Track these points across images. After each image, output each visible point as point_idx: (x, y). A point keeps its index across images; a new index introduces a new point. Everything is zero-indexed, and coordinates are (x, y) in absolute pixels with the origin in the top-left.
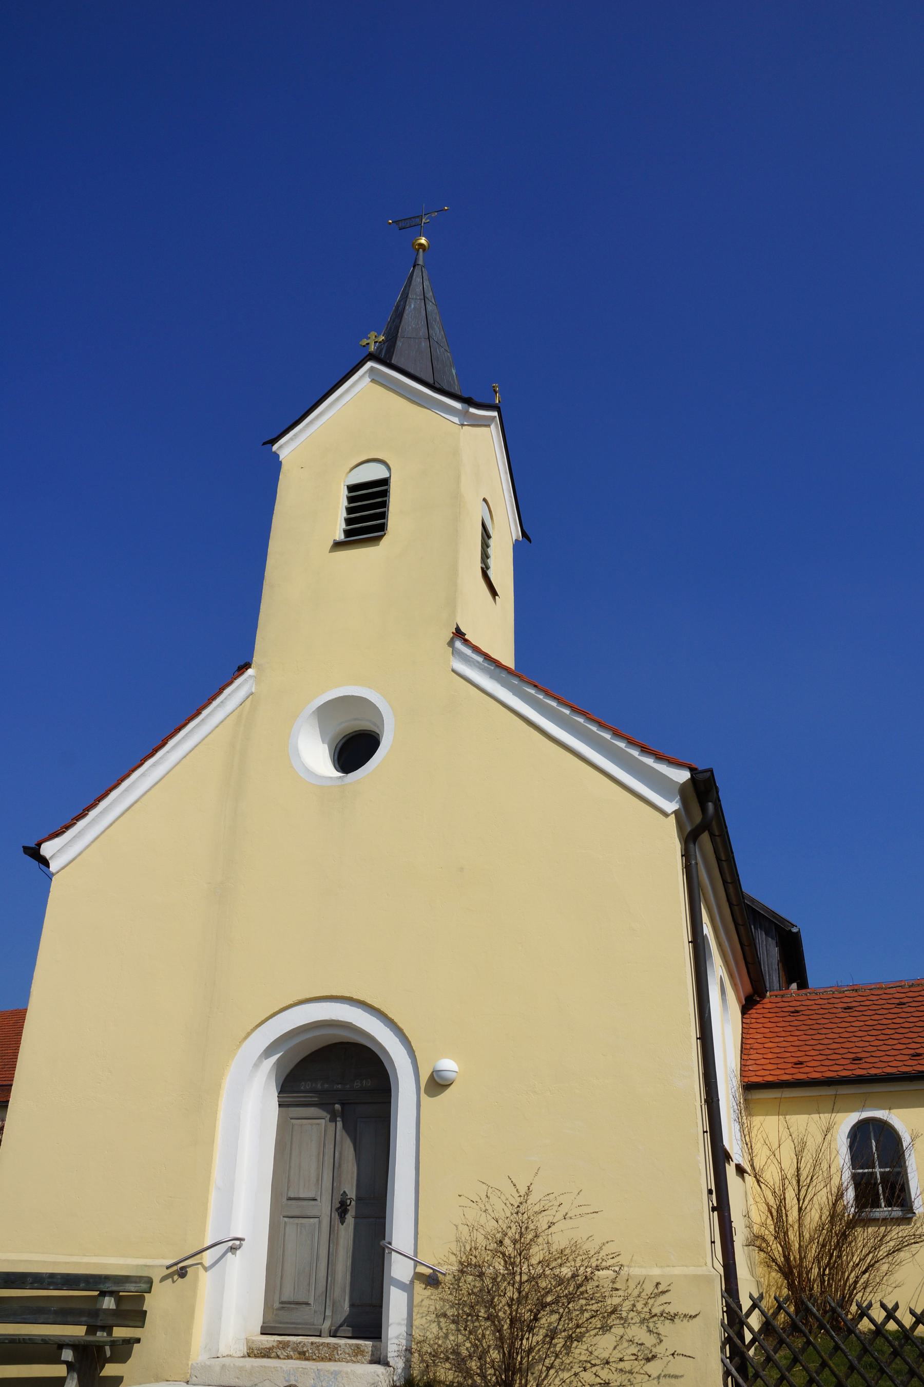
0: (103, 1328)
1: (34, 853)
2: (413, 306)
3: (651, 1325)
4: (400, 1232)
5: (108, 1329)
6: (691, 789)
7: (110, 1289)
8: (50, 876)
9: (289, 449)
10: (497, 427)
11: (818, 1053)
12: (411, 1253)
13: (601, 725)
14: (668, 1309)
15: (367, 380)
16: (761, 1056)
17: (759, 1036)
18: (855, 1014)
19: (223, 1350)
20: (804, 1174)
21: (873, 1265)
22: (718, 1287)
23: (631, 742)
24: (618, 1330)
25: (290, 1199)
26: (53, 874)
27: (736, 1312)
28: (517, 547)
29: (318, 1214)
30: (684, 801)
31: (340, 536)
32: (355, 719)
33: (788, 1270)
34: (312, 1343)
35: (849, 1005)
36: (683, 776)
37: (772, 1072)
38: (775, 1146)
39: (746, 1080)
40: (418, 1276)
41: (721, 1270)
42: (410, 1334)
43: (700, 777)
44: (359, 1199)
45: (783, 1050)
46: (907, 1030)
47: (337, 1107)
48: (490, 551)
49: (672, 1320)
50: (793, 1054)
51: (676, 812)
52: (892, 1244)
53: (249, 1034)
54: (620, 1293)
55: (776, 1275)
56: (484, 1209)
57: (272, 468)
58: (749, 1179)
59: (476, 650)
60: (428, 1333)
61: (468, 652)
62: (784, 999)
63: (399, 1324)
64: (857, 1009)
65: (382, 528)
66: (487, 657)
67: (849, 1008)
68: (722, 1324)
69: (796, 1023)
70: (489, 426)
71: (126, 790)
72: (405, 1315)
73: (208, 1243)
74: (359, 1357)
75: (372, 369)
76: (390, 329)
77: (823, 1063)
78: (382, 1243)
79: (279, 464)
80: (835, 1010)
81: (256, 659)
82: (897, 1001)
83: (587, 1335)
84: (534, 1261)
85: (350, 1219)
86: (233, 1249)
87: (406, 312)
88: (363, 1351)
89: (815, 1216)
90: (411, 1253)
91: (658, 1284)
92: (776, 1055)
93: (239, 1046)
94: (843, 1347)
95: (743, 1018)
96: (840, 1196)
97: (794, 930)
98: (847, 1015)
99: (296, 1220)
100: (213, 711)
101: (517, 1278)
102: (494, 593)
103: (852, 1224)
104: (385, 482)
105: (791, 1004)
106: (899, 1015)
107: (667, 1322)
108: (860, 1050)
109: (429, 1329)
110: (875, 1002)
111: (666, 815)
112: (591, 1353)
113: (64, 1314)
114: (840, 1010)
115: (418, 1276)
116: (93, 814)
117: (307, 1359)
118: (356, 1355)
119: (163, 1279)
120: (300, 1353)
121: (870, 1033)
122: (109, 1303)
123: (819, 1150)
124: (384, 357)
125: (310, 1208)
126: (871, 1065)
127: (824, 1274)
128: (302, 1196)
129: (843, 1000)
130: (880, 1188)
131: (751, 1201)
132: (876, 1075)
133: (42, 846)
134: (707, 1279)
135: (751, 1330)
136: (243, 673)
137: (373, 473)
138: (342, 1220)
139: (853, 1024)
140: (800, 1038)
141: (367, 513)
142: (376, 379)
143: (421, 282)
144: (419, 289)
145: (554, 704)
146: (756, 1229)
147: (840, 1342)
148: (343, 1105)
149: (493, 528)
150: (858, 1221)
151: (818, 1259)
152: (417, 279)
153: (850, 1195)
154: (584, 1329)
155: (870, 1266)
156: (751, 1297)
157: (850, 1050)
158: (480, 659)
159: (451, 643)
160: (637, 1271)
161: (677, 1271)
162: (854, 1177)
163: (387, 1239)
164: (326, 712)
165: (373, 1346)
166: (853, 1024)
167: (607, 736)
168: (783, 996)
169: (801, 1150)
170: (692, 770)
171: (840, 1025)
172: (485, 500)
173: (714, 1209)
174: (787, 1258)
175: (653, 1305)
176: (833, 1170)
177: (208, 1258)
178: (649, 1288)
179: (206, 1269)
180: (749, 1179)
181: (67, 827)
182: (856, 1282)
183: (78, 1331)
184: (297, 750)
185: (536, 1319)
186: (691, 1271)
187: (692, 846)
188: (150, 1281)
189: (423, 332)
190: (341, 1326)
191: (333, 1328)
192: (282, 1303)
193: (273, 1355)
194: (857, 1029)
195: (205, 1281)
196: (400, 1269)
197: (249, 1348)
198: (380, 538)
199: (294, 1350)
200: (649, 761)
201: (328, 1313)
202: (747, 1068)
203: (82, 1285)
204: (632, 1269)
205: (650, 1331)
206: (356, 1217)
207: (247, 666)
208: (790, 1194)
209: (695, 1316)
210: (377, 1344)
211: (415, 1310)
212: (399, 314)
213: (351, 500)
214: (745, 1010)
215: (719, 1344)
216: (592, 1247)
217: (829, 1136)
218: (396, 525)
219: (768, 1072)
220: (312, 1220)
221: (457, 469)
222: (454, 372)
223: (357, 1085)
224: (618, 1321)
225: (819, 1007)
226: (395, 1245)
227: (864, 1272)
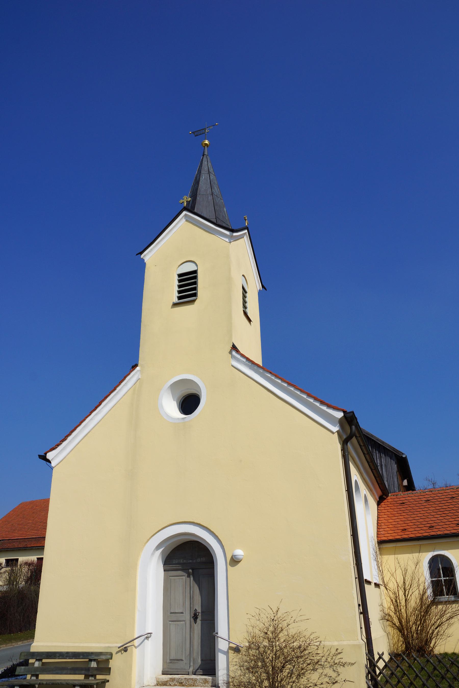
0: (92, 676)
1: (44, 458)
2: (204, 177)
3: (335, 668)
4: (222, 629)
5: (94, 676)
6: (344, 420)
7: (94, 658)
8: (52, 468)
9: (149, 256)
10: (247, 237)
11: (413, 524)
12: (227, 638)
13: (302, 391)
14: (342, 660)
15: (184, 220)
16: (387, 526)
17: (386, 516)
18: (431, 503)
19: (146, 683)
20: (407, 584)
21: (440, 625)
22: (364, 650)
23: (316, 399)
24: (320, 671)
25: (171, 613)
26: (53, 468)
27: (372, 661)
28: (260, 293)
29: (185, 620)
30: (342, 426)
31: (176, 300)
32: (188, 389)
33: (402, 629)
34: (185, 679)
35: (428, 499)
36: (340, 415)
37: (392, 535)
38: (394, 571)
39: (380, 539)
40: (230, 648)
41: (365, 640)
42: (228, 675)
43: (348, 415)
44: (202, 612)
45: (397, 523)
46: (455, 511)
47: (190, 571)
48: (247, 299)
49: (343, 666)
50: (401, 525)
51: (338, 432)
52: (448, 615)
53: (148, 540)
54: (319, 655)
55: (396, 631)
56: (258, 619)
57: (141, 266)
58: (382, 588)
59: (243, 356)
60: (236, 674)
61: (238, 356)
62: (397, 497)
63: (223, 669)
64: (432, 501)
65: (195, 295)
66: (248, 359)
67: (428, 501)
68: (366, 666)
69: (403, 509)
70: (243, 237)
71: (84, 427)
72: (226, 666)
73: (136, 637)
74: (206, 684)
75: (186, 215)
76: (193, 190)
77: (415, 529)
78: (214, 633)
79: (144, 264)
80: (421, 502)
81: (140, 362)
82: (450, 496)
83: (307, 673)
84: (282, 640)
85: (199, 621)
86: (147, 638)
87: (201, 181)
88: (208, 682)
89: (414, 601)
90: (227, 638)
91: (337, 649)
92: (393, 526)
93: (144, 546)
94: (420, 675)
95: (378, 507)
96: (424, 593)
97: (404, 456)
98: (427, 504)
99: (175, 623)
100: (122, 388)
101: (275, 648)
102: (250, 320)
103: (429, 607)
104: (195, 272)
105: (401, 499)
106: (452, 504)
107: (341, 667)
108: (433, 522)
109: (236, 672)
110: (440, 497)
111: (333, 433)
112: (308, 681)
113: (74, 670)
114: (424, 502)
115: (230, 648)
116: (69, 438)
117: (183, 686)
118: (205, 683)
119: (117, 653)
120: (180, 683)
121: (437, 513)
122: (94, 665)
123: (413, 573)
124: (191, 208)
125: (181, 617)
126: (438, 530)
127: (418, 630)
128: (177, 611)
129: (425, 496)
130: (444, 587)
131: (383, 597)
132: (440, 535)
133: (47, 454)
134: (359, 646)
135: (379, 668)
136: (135, 369)
137: (189, 268)
138: (195, 622)
139: (430, 509)
140: (405, 517)
141: (188, 287)
142: (188, 220)
143: (207, 164)
144: (206, 168)
145: (279, 381)
146: (386, 611)
147: (418, 673)
148: (193, 569)
149: (248, 288)
150: (434, 603)
151: (415, 623)
152: (205, 163)
153: (429, 592)
154: (305, 670)
155: (439, 626)
156: (378, 654)
157: (428, 522)
158: (244, 360)
159: (230, 352)
160: (327, 643)
161: (345, 643)
162: (432, 582)
163: (216, 631)
164: (175, 386)
165: (212, 679)
166: (430, 509)
167: (305, 396)
168: (397, 495)
169: (408, 571)
170: (344, 412)
171: (424, 510)
172: (243, 275)
173: (361, 613)
174: (400, 622)
175: (335, 659)
176: (420, 582)
177: (136, 643)
178: (333, 651)
179: (136, 647)
180: (382, 588)
181: (58, 445)
182: (432, 633)
183: (81, 677)
184: (162, 406)
185: (283, 667)
186: (352, 642)
187: (346, 446)
188: (111, 654)
189: (209, 191)
190: (197, 669)
191: (194, 671)
192: (171, 660)
193: (168, 684)
194: (432, 511)
195: (136, 653)
196: (222, 645)
197: (157, 681)
198: (194, 301)
199: (177, 682)
200: (324, 408)
201: (192, 664)
202: (380, 533)
203: (81, 657)
204: (325, 643)
205: (334, 671)
206: (201, 620)
207: (136, 366)
208: (401, 593)
209: (353, 664)
210: (214, 678)
211: (230, 663)
212: (197, 182)
213: (180, 281)
214: (379, 504)
215: (365, 675)
216: (307, 634)
217: (418, 567)
218: (203, 292)
219: (390, 535)
220: (182, 622)
221: (230, 262)
222: (225, 210)
223: (199, 560)
224: (320, 666)
225: (414, 500)
226: (219, 635)
227: (436, 628)
